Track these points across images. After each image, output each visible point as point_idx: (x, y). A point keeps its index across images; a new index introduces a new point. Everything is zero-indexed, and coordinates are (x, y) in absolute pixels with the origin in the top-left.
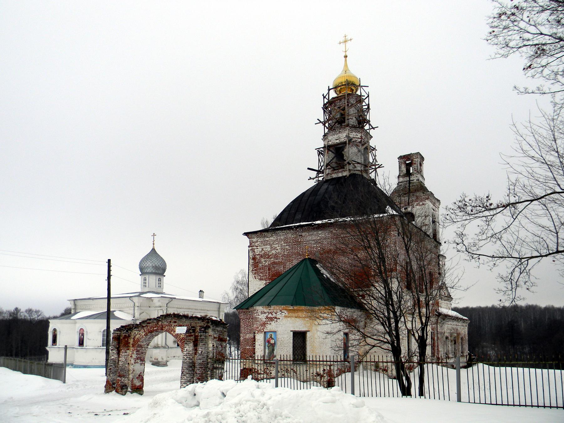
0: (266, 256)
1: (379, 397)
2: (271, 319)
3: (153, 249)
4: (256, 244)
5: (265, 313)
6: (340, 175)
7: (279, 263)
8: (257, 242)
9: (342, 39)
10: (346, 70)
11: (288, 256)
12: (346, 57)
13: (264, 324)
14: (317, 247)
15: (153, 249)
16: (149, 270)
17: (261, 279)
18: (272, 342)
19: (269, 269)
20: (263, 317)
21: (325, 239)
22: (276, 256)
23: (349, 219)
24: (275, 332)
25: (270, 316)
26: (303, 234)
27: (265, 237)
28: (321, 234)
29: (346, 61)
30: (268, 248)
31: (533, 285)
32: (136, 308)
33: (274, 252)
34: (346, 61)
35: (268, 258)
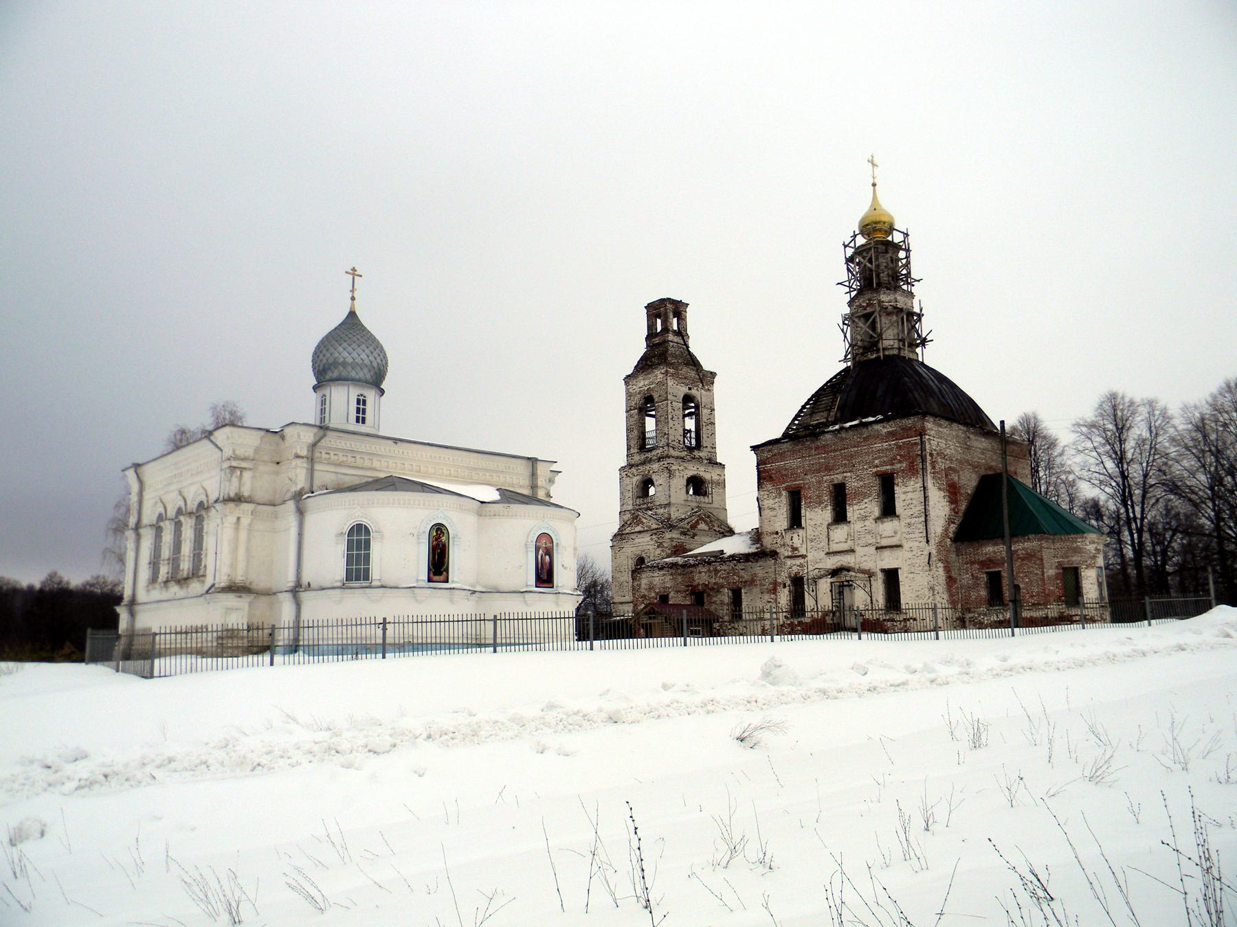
3: (352, 314)
10: (875, 206)
11: (960, 462)
12: (874, 185)
15: (352, 314)
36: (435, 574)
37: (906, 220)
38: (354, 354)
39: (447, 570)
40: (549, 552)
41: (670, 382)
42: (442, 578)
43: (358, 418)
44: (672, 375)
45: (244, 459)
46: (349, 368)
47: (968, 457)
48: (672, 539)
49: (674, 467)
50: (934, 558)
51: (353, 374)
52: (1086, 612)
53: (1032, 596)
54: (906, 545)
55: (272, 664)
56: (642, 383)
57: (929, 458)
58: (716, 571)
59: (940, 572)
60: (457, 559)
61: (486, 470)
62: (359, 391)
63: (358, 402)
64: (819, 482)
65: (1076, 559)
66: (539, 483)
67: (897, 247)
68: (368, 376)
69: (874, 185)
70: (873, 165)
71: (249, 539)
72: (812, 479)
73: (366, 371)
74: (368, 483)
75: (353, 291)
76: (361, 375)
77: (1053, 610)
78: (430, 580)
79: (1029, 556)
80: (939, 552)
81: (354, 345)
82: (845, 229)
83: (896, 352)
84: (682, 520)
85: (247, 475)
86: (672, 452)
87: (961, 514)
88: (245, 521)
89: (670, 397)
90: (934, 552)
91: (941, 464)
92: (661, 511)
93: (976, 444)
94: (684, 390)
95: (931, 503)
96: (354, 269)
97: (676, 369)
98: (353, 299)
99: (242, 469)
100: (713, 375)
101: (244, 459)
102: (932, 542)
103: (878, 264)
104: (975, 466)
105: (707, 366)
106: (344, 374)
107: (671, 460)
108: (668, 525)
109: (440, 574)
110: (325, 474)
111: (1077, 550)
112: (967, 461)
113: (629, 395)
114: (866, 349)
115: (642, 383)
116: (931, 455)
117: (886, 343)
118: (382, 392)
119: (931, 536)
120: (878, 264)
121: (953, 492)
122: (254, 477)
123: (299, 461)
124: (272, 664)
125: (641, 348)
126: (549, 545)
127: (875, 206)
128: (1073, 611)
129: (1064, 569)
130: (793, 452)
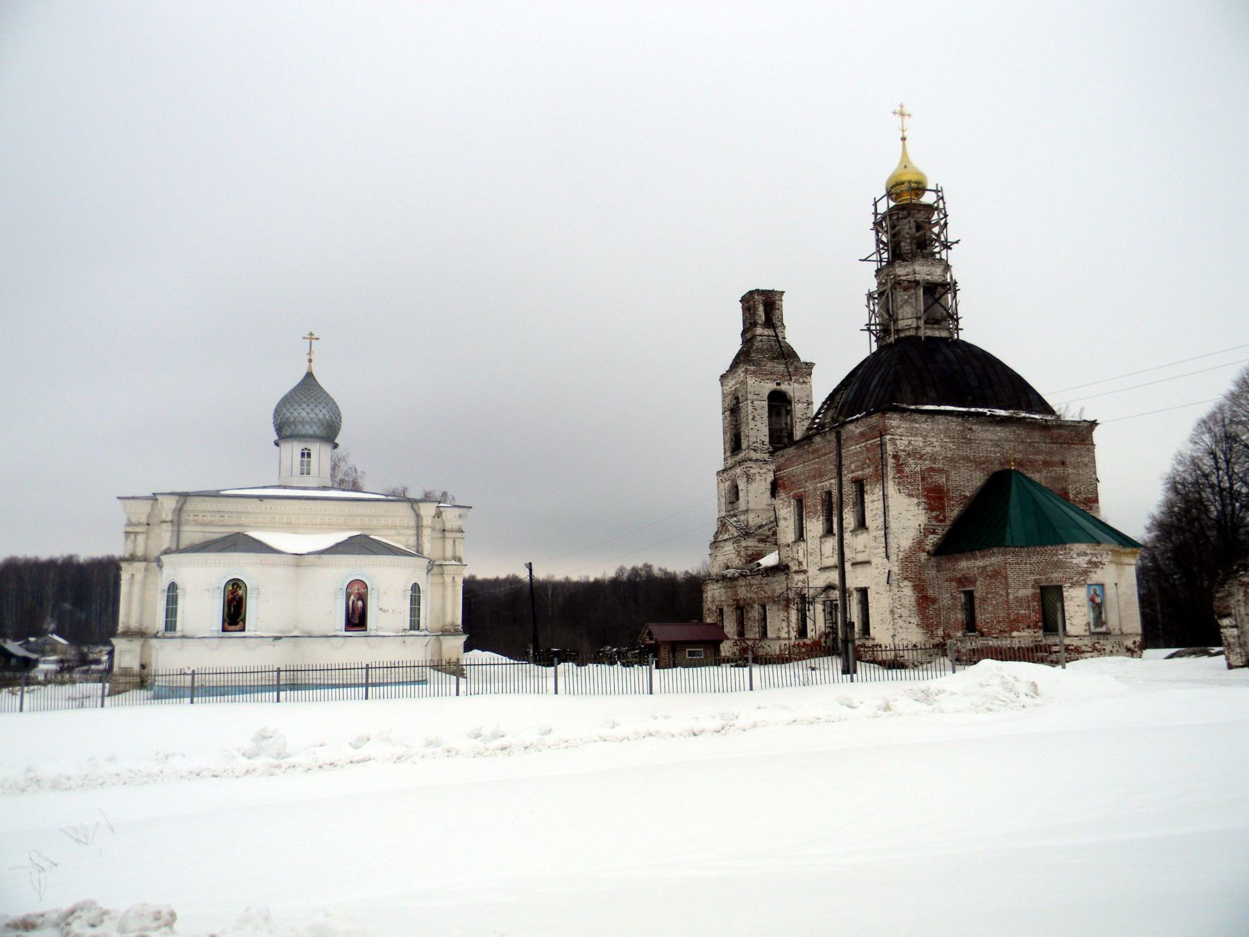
0: (915, 454)
1: (776, 689)
2: (1096, 565)
3: (309, 375)
4: (898, 431)
5: (1086, 554)
6: (937, 334)
7: (940, 471)
8: (899, 427)
9: (906, 110)
10: (905, 164)
11: (952, 460)
12: (904, 139)
13: (1085, 572)
14: (995, 453)
15: (309, 375)
16: (310, 430)
17: (910, 495)
18: (1098, 600)
19: (923, 479)
20: (1082, 562)
21: (1006, 440)
22: (933, 458)
23: (1037, 417)
24: (1102, 585)
25: (1094, 559)
26: (974, 427)
27: (915, 421)
28: (1000, 433)
29: (904, 146)
30: (919, 442)
31: (444, 494)
32: (426, 532)
33: (929, 449)
34: (904, 146)
35: (920, 458)
36: (230, 624)
37: (939, 173)
38: (317, 411)
39: (244, 620)
40: (363, 597)
41: (751, 381)
42: (238, 627)
43: (302, 470)
44: (754, 373)
45: (139, 524)
46: (300, 426)
47: (969, 453)
48: (746, 548)
49: (752, 471)
50: (893, 577)
51: (303, 432)
52: (1067, 641)
53: (999, 622)
54: (874, 561)
55: (102, 706)
56: (731, 383)
57: (891, 461)
58: (751, 585)
59: (908, 592)
60: (253, 609)
61: (365, 516)
62: (303, 446)
63: (303, 455)
64: (815, 490)
65: (1056, 576)
66: (425, 523)
67: (930, 209)
68: (318, 432)
69: (904, 139)
70: (902, 114)
71: (143, 593)
72: (810, 486)
73: (315, 428)
74: (215, 542)
75: (309, 354)
76: (311, 432)
77: (1023, 637)
78: (224, 630)
79: (996, 574)
80: (904, 568)
81: (312, 406)
82: (866, 197)
83: (912, 333)
84: (761, 527)
85: (141, 538)
86: (754, 455)
87: (948, 522)
88: (139, 577)
89: (750, 396)
90: (895, 569)
91: (913, 466)
92: (742, 518)
93: (983, 435)
94: (769, 386)
95: (893, 513)
96: (311, 334)
97: (759, 365)
98: (310, 361)
99: (136, 534)
100: (810, 366)
101: (139, 524)
102: (893, 558)
103: (910, 226)
104: (978, 463)
105: (804, 357)
106: (296, 432)
107: (749, 464)
108: (746, 533)
109: (236, 624)
110: (192, 534)
111: (1058, 565)
112: (967, 459)
113: (724, 396)
114: (886, 331)
115: (731, 383)
116: (895, 457)
117: (901, 324)
118: (336, 446)
119: (893, 550)
120: (910, 226)
121: (934, 498)
122: (147, 539)
123: (164, 525)
124: (102, 706)
125: (736, 345)
126: (363, 591)
127: (905, 164)
128: (1051, 640)
129: (1042, 588)
130: (799, 456)
